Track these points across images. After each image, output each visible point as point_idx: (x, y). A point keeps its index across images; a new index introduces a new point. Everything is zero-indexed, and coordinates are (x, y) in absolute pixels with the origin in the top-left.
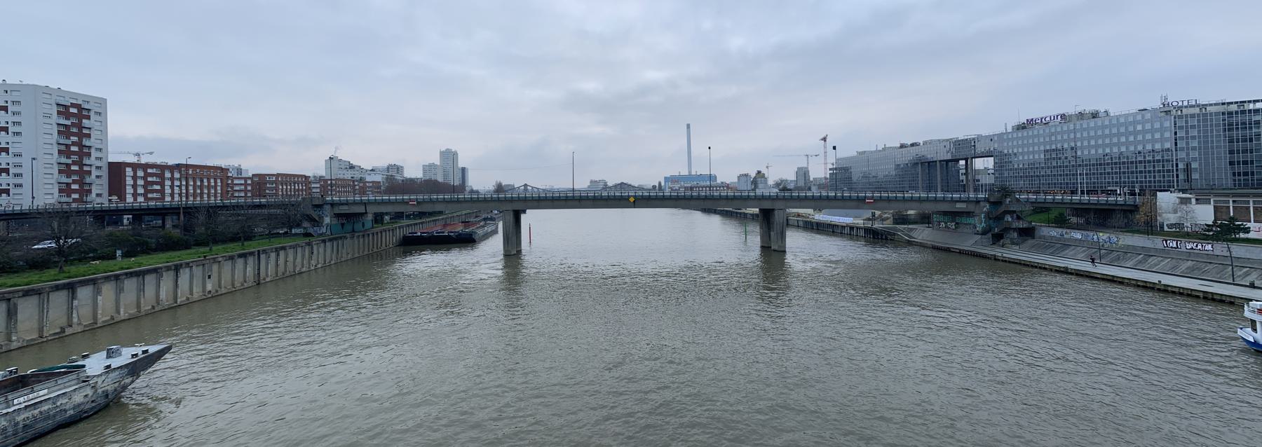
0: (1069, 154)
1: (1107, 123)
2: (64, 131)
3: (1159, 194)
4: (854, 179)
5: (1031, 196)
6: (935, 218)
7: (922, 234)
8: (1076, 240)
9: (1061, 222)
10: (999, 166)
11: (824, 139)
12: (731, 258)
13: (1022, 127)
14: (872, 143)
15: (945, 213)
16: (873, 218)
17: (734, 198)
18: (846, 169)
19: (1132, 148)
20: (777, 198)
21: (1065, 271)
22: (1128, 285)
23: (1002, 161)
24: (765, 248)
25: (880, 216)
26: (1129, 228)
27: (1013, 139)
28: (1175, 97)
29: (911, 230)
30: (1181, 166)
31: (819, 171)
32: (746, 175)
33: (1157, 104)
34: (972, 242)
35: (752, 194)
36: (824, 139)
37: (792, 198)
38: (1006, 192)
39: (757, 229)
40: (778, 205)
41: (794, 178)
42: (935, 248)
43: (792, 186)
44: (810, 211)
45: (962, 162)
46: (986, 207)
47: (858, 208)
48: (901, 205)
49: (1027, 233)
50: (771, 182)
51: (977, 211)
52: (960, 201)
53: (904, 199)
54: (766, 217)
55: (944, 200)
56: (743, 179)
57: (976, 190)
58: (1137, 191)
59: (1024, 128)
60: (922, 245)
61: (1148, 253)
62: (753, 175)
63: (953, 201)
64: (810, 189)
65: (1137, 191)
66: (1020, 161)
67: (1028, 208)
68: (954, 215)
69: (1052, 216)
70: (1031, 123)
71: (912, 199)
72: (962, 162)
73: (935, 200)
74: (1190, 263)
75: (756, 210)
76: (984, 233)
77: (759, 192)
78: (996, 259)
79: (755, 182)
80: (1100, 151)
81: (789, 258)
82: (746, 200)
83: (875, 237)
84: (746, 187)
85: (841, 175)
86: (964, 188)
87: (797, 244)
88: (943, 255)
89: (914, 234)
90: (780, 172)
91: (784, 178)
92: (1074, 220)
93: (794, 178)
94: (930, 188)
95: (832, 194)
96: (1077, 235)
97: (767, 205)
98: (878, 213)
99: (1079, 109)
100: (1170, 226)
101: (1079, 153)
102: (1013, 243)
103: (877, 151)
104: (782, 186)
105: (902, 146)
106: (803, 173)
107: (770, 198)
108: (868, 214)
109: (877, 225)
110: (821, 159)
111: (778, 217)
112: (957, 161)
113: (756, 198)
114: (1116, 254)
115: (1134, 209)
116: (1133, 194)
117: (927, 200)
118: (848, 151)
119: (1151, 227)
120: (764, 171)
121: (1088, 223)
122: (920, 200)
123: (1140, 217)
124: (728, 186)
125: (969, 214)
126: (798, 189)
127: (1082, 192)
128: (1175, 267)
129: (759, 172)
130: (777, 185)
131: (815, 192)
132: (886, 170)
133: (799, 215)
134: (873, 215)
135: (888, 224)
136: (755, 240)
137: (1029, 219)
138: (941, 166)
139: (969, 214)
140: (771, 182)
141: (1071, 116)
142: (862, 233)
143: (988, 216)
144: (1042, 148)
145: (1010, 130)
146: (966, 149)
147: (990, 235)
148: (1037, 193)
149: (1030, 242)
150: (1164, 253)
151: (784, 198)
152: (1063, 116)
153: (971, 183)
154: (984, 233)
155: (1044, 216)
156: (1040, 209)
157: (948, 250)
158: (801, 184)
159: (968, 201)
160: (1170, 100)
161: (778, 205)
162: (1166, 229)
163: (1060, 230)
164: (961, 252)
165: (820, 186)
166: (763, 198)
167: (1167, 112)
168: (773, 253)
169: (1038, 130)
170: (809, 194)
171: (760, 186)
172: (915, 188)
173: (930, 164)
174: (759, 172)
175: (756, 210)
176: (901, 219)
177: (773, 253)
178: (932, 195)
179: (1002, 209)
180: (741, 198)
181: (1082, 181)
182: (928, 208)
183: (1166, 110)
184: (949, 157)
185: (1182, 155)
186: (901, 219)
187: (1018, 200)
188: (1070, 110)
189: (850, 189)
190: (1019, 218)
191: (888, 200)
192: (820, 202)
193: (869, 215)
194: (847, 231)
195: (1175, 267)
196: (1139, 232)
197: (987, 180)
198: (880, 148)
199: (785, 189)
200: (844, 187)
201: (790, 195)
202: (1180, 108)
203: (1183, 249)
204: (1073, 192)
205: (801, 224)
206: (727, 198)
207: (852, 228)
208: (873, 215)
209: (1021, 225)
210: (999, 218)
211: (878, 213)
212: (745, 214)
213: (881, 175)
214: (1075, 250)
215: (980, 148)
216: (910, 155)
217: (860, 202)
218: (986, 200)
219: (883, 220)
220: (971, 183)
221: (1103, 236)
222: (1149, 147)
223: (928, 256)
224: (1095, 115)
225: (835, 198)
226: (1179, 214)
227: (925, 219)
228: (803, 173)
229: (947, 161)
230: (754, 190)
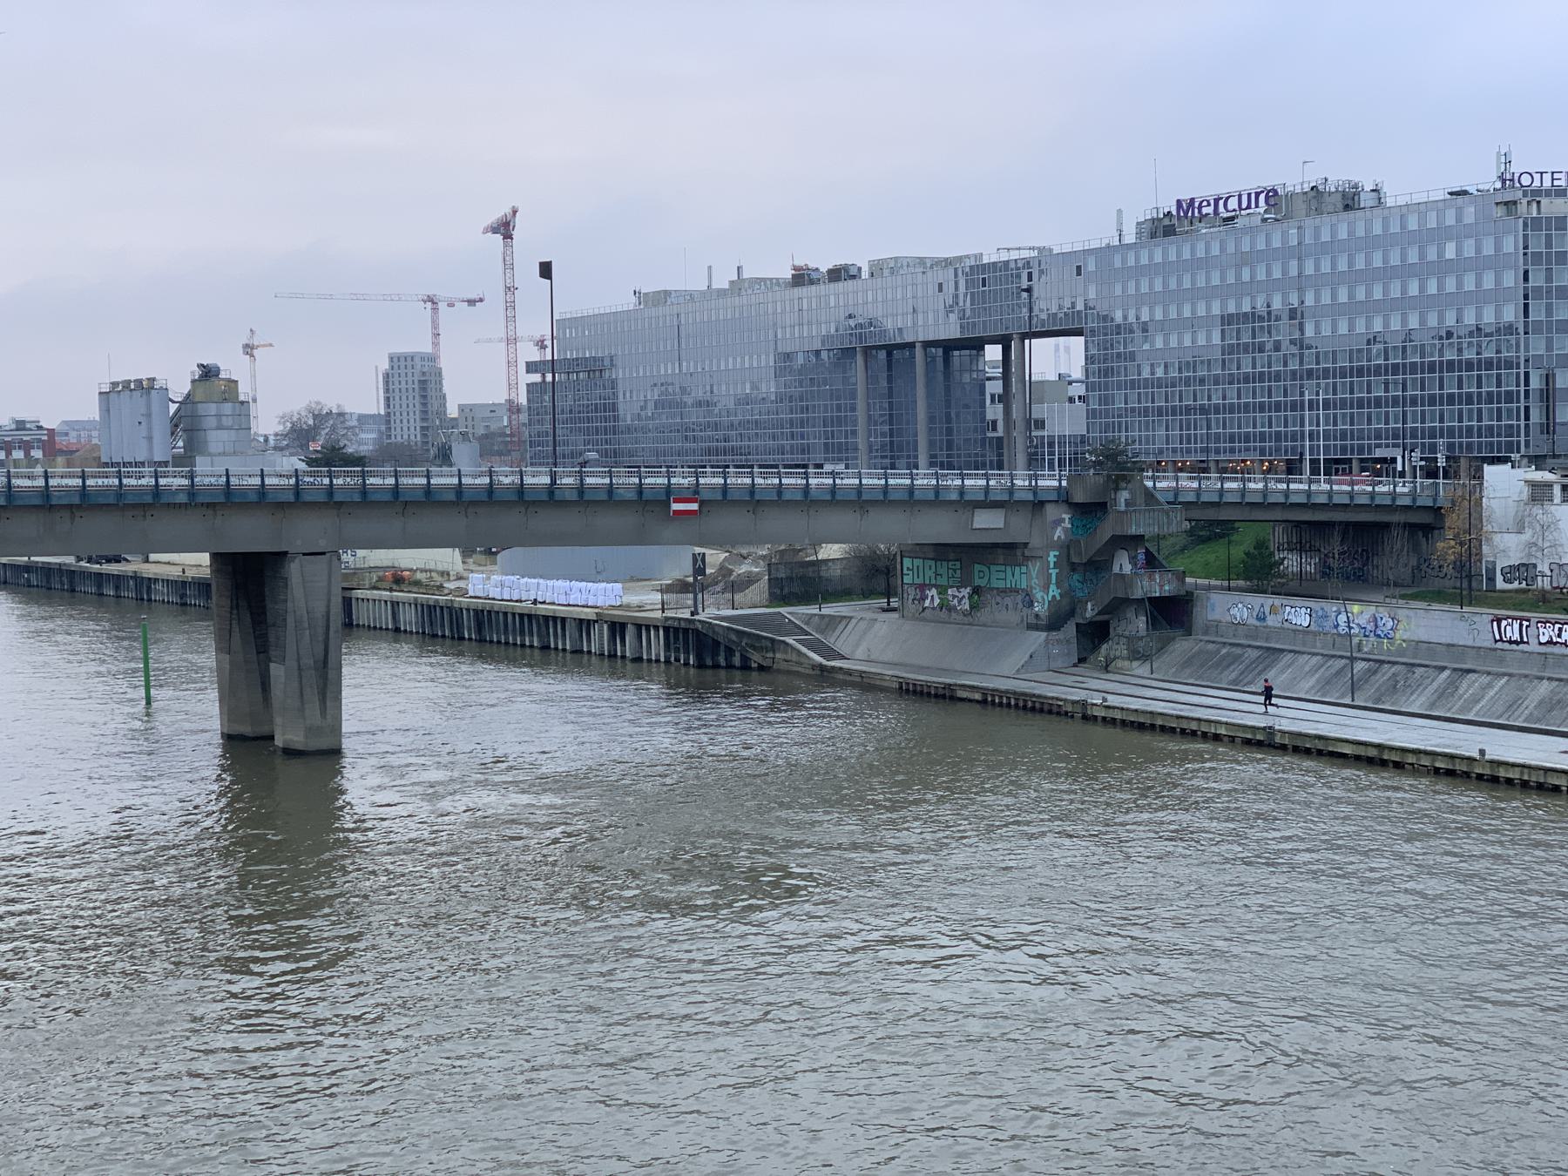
0: (1284, 332)
1: (1377, 229)
2: (139, 382)
3: (1488, 470)
4: (628, 410)
5: (1188, 483)
6: (911, 572)
7: (869, 637)
8: (1297, 631)
9: (1259, 574)
10: (1102, 367)
11: (504, 229)
12: (82, 814)
13: (1162, 228)
14: (693, 261)
15: (942, 552)
16: (697, 583)
17: (85, 503)
18: (596, 368)
19: (1432, 321)
20: (295, 501)
21: (1265, 742)
22: (1416, 771)
23: (1109, 344)
24: (246, 746)
25: (724, 571)
26: (1422, 586)
27: (1139, 271)
28: (1538, 160)
29: (832, 622)
30: (1536, 383)
31: (484, 376)
32: (145, 388)
33: (1483, 178)
34: (1018, 658)
35: (175, 481)
36: (504, 229)
37: (365, 500)
38: (1117, 466)
39: (208, 658)
40: (302, 533)
41: (372, 403)
42: (912, 692)
43: (364, 443)
44: (446, 558)
45: (993, 352)
46: (1061, 524)
47: (640, 538)
48: (787, 527)
49: (1172, 613)
50: (267, 422)
51: (1036, 542)
52: (987, 502)
53: (807, 501)
54: (248, 591)
55: (937, 501)
56: (129, 406)
57: (1034, 461)
58: (1441, 463)
59: (1169, 231)
60: (865, 684)
61: (1458, 663)
62: (180, 386)
63: (967, 504)
64: (445, 456)
65: (1441, 463)
66: (1158, 353)
67: (1178, 524)
68: (965, 558)
69: (1238, 552)
70: (1188, 210)
71: (834, 499)
72: (993, 352)
73: (911, 501)
74: (1544, 688)
75: (198, 563)
76: (1054, 624)
77: (208, 472)
78: (1084, 715)
79: (188, 423)
80: (1360, 327)
81: (361, 787)
82: (145, 510)
83: (705, 660)
84: (144, 448)
85: (575, 390)
86: (995, 455)
87: (389, 703)
88: (934, 717)
89: (841, 641)
90: (309, 378)
91: (331, 404)
92: (1291, 562)
93: (372, 403)
94: (894, 453)
95: (538, 479)
96: (1299, 615)
97: (250, 535)
98: (715, 558)
99: (1312, 178)
100: (1511, 572)
101: (1309, 331)
102: (1136, 655)
103: (711, 294)
104: (322, 442)
105: (802, 278)
106: (415, 380)
107: (262, 500)
108: (678, 565)
109: (714, 611)
110: (491, 317)
111: (304, 593)
112: (977, 345)
113: (197, 502)
114: (1388, 671)
115: (1424, 524)
116: (1431, 473)
117: (885, 499)
118: (599, 289)
119: (1467, 584)
120: (232, 366)
121: (1326, 571)
122: (860, 501)
123: (1445, 547)
124: (50, 443)
125: (1009, 552)
126: (393, 454)
127: (1315, 471)
128: (1512, 706)
129: (208, 373)
130: (298, 436)
131: (468, 470)
132: (743, 377)
133: (398, 580)
134: (699, 566)
135: (752, 604)
136: (196, 711)
137: (1179, 565)
138: (930, 362)
139: (1009, 552)
140: (267, 422)
141: (1291, 196)
142: (656, 646)
143: (1069, 564)
144: (1216, 310)
145: (1130, 238)
146: (1004, 301)
147: (1070, 630)
148: (1201, 469)
149: (1182, 646)
150: (1493, 657)
151: (331, 502)
152: (1271, 194)
153: (1018, 434)
154: (1054, 624)
155: (1214, 553)
156: (1210, 526)
157: (946, 696)
158: (407, 431)
159: (1006, 503)
160: (1516, 168)
161: (302, 533)
162: (1500, 584)
163: (1256, 600)
164: (990, 701)
165: (492, 445)
166: (229, 499)
167: (1510, 205)
168: (279, 766)
169: (1206, 241)
170: (443, 479)
171: (217, 440)
172: (842, 452)
173: (891, 356)
174: (208, 373)
175: (198, 563)
176: (798, 583)
177: (279, 766)
178: (899, 481)
179: (1107, 530)
180: (120, 504)
181: (1316, 430)
182: (889, 532)
183: (1514, 198)
184: (951, 331)
185: (1537, 346)
186: (798, 583)
187: (1150, 496)
188: (1293, 178)
189: (612, 458)
190: (1151, 562)
191: (753, 501)
192: (488, 518)
193: (684, 570)
194: (599, 639)
195: (1512, 706)
196: (1440, 596)
197: (1065, 422)
198: (721, 282)
199: (333, 458)
200: (587, 446)
201: (366, 482)
202: (1535, 195)
203: (1533, 647)
204: (1292, 468)
205: (409, 618)
206: (46, 503)
207: (617, 628)
208: (699, 566)
209: (1159, 586)
210: (1097, 566)
211: (715, 558)
212: (144, 585)
213: (726, 395)
214: (1301, 666)
215: (1049, 300)
216: (826, 315)
217: (649, 512)
218: (1063, 498)
219: (738, 586)
220: (1018, 434)
221: (1360, 613)
222: (1470, 319)
223: (886, 718)
224: (1349, 200)
225: (551, 498)
226: (1527, 536)
227: (876, 578)
228: (415, 380)
229: (948, 346)
230: (185, 460)
